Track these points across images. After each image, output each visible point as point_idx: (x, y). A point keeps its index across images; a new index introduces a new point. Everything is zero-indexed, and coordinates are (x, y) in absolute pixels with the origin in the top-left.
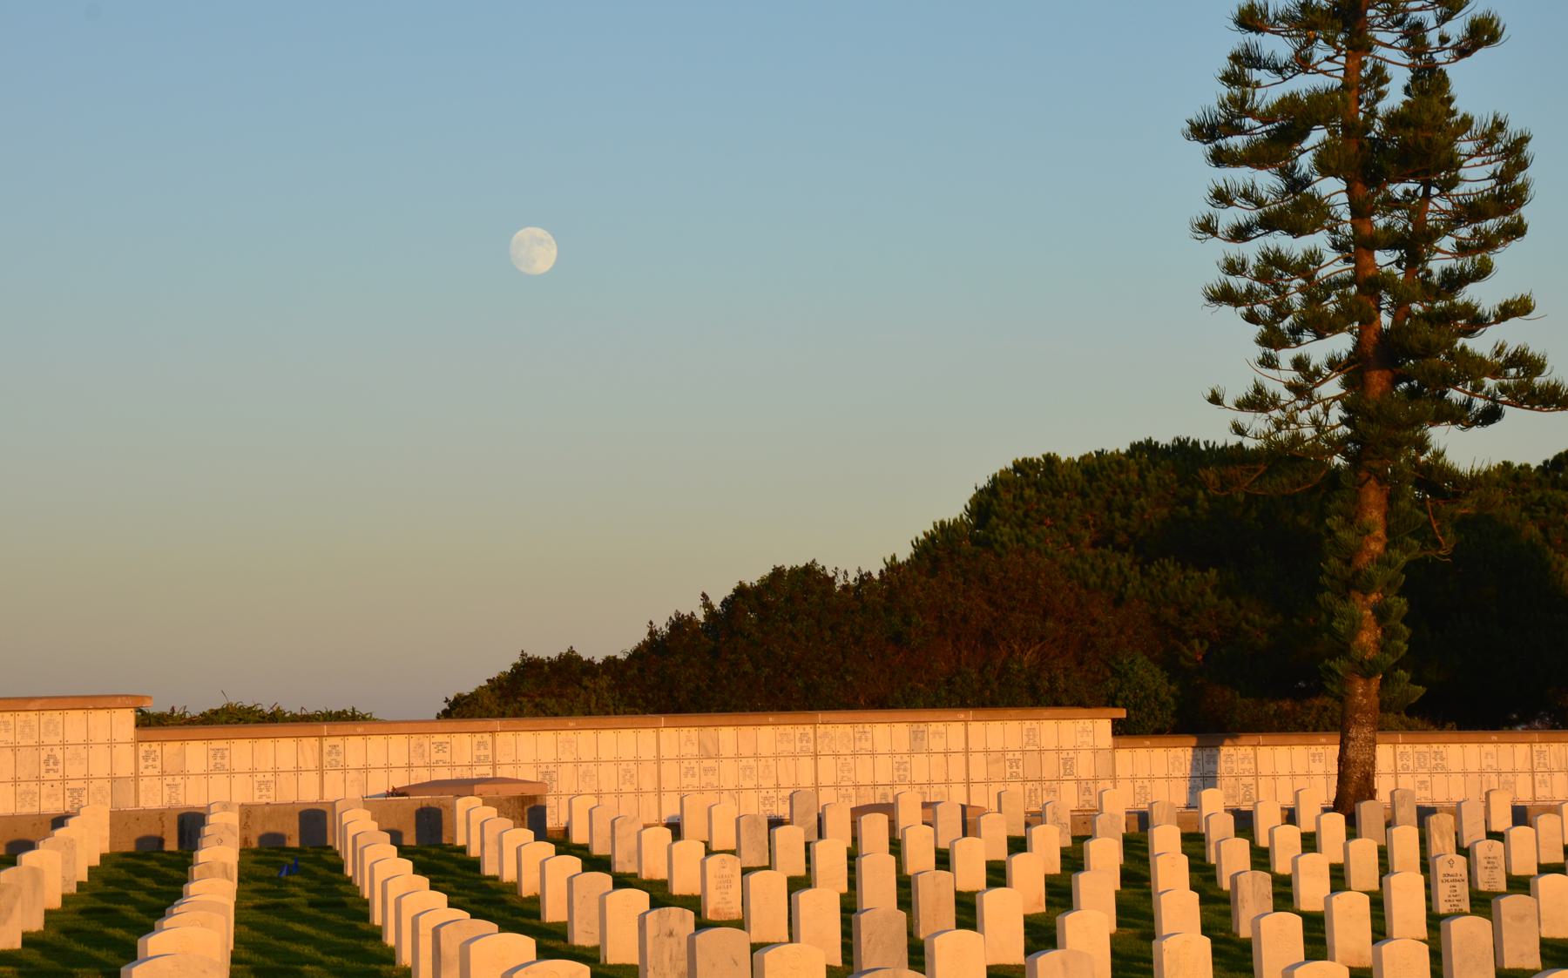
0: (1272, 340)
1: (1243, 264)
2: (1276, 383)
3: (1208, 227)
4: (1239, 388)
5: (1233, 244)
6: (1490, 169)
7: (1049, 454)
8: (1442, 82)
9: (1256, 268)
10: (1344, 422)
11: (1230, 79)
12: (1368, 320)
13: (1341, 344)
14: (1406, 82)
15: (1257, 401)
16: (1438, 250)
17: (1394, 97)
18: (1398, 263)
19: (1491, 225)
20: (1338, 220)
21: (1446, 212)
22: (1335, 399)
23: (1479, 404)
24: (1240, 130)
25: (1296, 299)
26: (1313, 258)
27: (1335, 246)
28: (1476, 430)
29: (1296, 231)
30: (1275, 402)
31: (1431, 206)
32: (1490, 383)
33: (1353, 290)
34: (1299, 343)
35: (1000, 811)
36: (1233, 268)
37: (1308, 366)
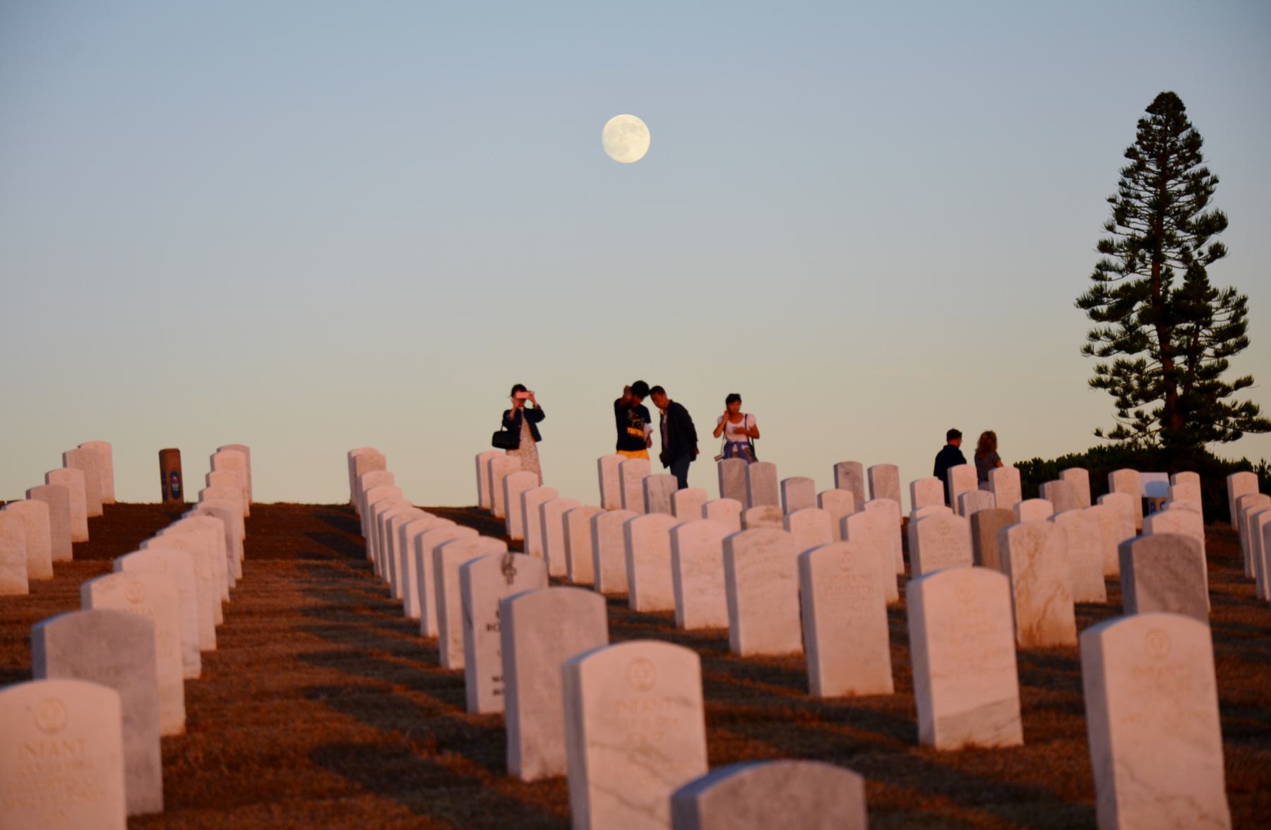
0: (1123, 405)
1: (1106, 368)
2: (1128, 424)
3: (1088, 350)
4: (1112, 428)
5: (1101, 358)
6: (1227, 315)
7: (1036, 459)
8: (1202, 273)
9: (1113, 371)
10: (1161, 442)
11: (1097, 277)
12: (1172, 392)
13: (1159, 404)
14: (1185, 274)
15: (1119, 433)
16: (1204, 355)
17: (1178, 281)
18: (1185, 363)
19: (1231, 342)
20: (1153, 344)
21: (1210, 337)
22: (1157, 431)
23: (1230, 431)
24: (1102, 303)
25: (1135, 383)
26: (1141, 363)
27: (1153, 356)
28: (1229, 443)
29: (1131, 351)
30: (1128, 434)
31: (1200, 334)
32: (1232, 420)
33: (1162, 378)
34: (1137, 405)
35: (624, 506)
36: (1101, 370)
37: (1142, 416)
